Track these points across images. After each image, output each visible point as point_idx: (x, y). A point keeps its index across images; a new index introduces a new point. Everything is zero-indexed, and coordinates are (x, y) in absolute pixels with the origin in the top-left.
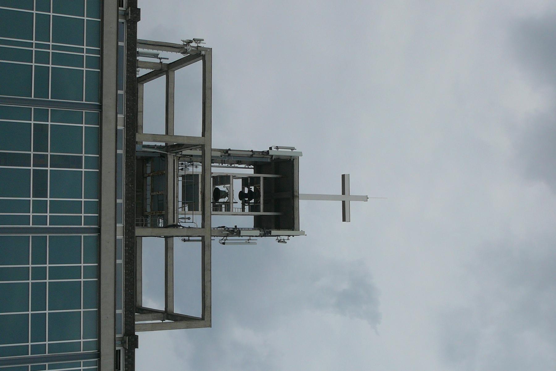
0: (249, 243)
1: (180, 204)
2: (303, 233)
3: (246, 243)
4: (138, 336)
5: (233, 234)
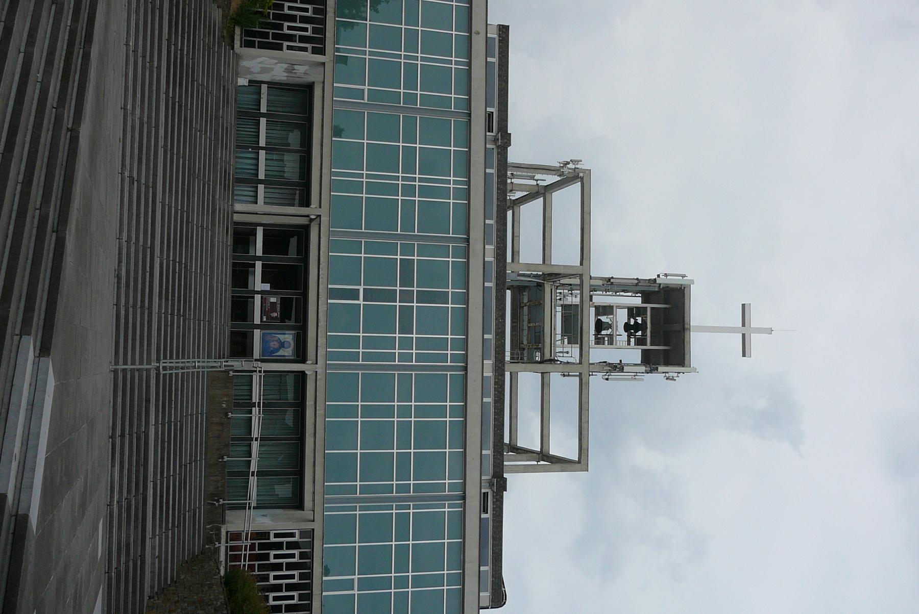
0: (635, 379)
1: (559, 337)
2: (695, 370)
3: (632, 378)
4: (506, 479)
5: (615, 370)
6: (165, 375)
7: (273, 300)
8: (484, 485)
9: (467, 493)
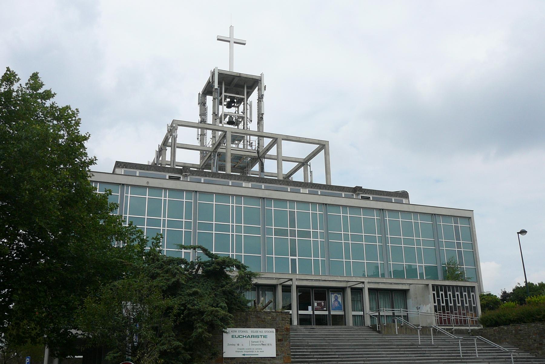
6: (463, 356)
7: (316, 304)
8: (186, 179)
9: (381, 208)
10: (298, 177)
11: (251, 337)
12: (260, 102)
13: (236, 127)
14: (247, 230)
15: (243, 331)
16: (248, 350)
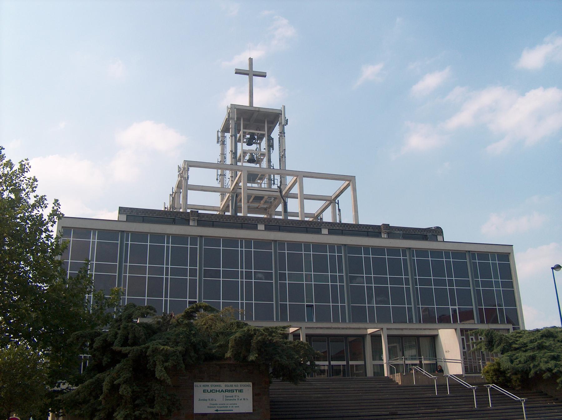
10: (327, 217)
11: (225, 392)
12: (281, 137)
13: (258, 166)
14: (300, 277)
15: (216, 386)
16: (221, 406)
